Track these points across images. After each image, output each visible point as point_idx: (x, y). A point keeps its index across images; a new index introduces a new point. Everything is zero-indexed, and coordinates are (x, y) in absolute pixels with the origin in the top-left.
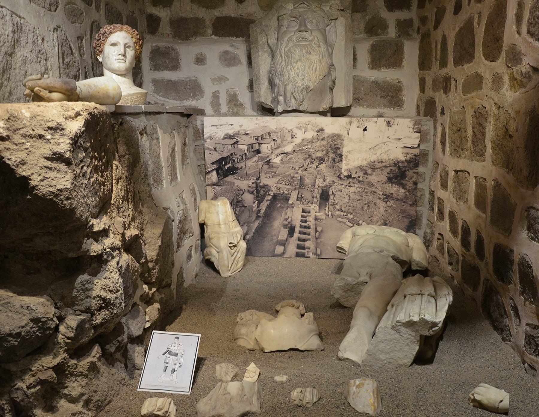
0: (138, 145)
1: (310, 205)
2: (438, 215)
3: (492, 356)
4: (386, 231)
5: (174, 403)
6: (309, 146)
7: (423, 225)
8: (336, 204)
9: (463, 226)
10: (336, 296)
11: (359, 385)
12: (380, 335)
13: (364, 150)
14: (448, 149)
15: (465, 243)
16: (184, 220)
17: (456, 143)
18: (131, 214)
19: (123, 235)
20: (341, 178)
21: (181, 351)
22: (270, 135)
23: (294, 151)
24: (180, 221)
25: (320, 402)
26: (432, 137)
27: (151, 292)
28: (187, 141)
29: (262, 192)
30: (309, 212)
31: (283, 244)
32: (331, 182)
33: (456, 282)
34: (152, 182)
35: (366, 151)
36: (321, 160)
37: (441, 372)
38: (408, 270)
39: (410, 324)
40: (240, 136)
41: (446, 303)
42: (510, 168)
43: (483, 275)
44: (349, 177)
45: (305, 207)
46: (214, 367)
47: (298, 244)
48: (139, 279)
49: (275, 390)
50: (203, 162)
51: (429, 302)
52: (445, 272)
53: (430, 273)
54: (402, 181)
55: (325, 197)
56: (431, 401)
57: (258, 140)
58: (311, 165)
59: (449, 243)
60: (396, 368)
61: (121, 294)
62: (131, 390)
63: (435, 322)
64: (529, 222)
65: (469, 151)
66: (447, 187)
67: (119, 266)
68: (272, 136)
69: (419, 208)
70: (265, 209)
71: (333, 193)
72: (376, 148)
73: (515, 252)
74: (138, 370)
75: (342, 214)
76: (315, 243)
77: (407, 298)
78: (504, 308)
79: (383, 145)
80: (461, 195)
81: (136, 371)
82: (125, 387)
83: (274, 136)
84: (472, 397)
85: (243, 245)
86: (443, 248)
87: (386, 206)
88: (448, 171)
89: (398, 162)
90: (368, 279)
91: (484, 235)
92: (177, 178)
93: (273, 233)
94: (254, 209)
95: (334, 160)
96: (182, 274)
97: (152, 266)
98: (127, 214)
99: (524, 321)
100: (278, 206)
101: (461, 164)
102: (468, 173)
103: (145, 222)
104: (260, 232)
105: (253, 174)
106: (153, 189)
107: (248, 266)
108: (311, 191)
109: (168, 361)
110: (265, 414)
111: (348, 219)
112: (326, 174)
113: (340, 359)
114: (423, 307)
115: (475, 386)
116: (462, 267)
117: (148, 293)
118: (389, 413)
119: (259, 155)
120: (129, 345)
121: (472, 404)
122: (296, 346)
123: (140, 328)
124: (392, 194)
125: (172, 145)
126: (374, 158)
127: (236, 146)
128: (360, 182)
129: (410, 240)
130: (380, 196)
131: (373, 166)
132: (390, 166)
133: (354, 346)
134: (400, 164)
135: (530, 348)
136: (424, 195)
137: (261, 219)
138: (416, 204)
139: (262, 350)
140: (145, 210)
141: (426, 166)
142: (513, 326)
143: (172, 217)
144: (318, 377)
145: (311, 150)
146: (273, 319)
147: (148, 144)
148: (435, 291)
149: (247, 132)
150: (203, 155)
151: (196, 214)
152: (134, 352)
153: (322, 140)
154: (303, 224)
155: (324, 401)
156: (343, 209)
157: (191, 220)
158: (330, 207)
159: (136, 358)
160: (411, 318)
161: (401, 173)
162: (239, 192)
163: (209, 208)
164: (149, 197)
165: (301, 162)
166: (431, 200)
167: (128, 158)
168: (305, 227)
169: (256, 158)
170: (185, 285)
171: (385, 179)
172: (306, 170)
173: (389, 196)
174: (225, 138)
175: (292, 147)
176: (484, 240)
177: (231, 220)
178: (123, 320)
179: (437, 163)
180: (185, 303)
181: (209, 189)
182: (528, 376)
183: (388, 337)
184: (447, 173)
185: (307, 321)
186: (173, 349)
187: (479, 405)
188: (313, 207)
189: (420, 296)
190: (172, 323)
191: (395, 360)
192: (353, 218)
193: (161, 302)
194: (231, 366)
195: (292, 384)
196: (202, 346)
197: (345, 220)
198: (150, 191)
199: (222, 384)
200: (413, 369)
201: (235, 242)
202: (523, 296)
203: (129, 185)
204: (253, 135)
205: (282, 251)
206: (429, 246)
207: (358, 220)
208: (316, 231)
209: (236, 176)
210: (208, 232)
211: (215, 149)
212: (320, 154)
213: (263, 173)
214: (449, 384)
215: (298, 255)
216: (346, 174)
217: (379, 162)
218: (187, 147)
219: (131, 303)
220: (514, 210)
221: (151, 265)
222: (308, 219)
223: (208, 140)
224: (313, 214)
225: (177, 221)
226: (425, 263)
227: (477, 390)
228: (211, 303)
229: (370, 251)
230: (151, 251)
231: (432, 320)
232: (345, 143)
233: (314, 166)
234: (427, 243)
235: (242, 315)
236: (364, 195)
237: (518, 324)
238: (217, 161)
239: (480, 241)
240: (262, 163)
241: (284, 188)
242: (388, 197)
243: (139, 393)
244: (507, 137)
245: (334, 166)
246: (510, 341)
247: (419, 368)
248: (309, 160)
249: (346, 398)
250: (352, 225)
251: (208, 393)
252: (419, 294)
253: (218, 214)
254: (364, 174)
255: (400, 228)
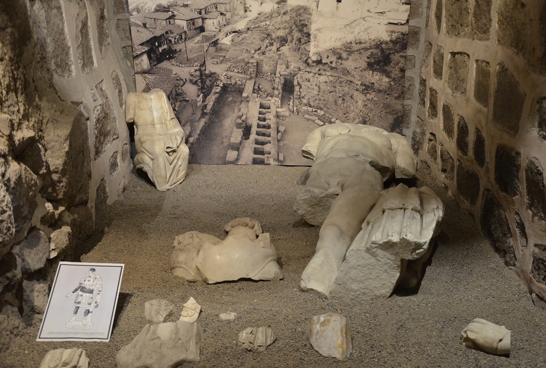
0: (25, 13)
1: (270, 98)
2: (430, 110)
3: (492, 284)
4: (364, 130)
5: (87, 354)
6: (268, 23)
7: (412, 123)
8: (303, 97)
9: (459, 123)
10: (300, 212)
11: (324, 322)
12: (352, 260)
13: (338, 27)
14: (444, 25)
15: (462, 145)
16: (104, 117)
17: (455, 17)
18: (22, 109)
19: (10, 137)
20: (308, 64)
21: (98, 286)
22: (216, 8)
23: (248, 29)
24: (98, 120)
25: (276, 345)
26: (425, 10)
27: (57, 212)
28: (106, 14)
29: (208, 83)
30: (269, 108)
31: (237, 148)
32: (296, 69)
33: (450, 193)
34: (53, 67)
35: (340, 28)
36: (283, 41)
37: (427, 304)
38: (390, 178)
39: (388, 246)
40: (177, 8)
41: (433, 220)
42: (520, 47)
43: (483, 183)
44: (319, 62)
45: (264, 102)
46: (142, 305)
47: (255, 148)
48: (39, 196)
49: (220, 330)
50: (129, 43)
51: (413, 218)
52: (437, 181)
53: (419, 183)
54: (386, 67)
55: (288, 88)
56: (413, 340)
57: (200, 13)
58: (270, 48)
59: (442, 145)
60: (372, 300)
61: (10, 216)
62: (28, 342)
63: (419, 243)
64: (541, 116)
65: (470, 27)
66: (441, 75)
67: (6, 178)
68: (219, 9)
69: (406, 102)
70: (212, 103)
71: (298, 83)
72: (353, 25)
73: (522, 155)
74: (38, 313)
75: (310, 109)
76: (276, 147)
77: (386, 213)
78: (508, 225)
79: (362, 21)
80: (458, 84)
81: (36, 315)
82: (18, 337)
83: (222, 8)
84: (465, 336)
85: (185, 150)
86: (436, 151)
87: (365, 99)
88: (443, 54)
89: (381, 43)
90: (339, 190)
91: (484, 134)
92: (92, 63)
93: (224, 135)
94: (199, 104)
95: (299, 40)
96: (105, 187)
97: (57, 179)
98: (16, 109)
99: (532, 241)
100: (230, 100)
101: (460, 44)
102: (468, 55)
103: (45, 121)
104: (207, 133)
105: (196, 59)
106: (56, 76)
107: (192, 177)
108: (271, 81)
109: (80, 300)
110: (206, 362)
111: (317, 116)
112: (289, 59)
113: (303, 291)
114: (405, 224)
115: (468, 322)
116: (458, 174)
117: (53, 213)
118: (361, 356)
119: (203, 34)
120: (25, 283)
121: (464, 344)
122: (248, 275)
123: (41, 259)
124: (373, 84)
125: (82, 17)
126: (350, 38)
127: (172, 21)
128: (332, 68)
129: (393, 141)
130: (358, 87)
131: (349, 49)
132: (371, 48)
133: (320, 274)
134: (383, 46)
135: (539, 274)
136: (414, 85)
137: (207, 117)
138: (403, 97)
139: (205, 281)
140: (44, 104)
141: (417, 48)
142: (518, 247)
143: (86, 115)
144: (275, 314)
145: (270, 28)
146: (219, 242)
147: (44, 15)
148: (422, 204)
149: (186, 3)
150: (128, 33)
151: (123, 111)
152: (32, 291)
153: (284, 14)
154: (262, 123)
155: (280, 344)
156: (312, 104)
157: (114, 118)
158: (296, 101)
159: (36, 298)
160: (390, 238)
161: (383, 57)
162: (179, 82)
163: (139, 103)
164: (50, 87)
165: (257, 43)
166: (422, 92)
167: (12, 32)
168: (264, 127)
169: (199, 38)
170: (109, 202)
171: (364, 65)
172: (264, 53)
173: (369, 87)
174: (157, 11)
175: (246, 23)
176: (484, 140)
177: (169, 118)
178: (16, 250)
179: (431, 44)
180: (108, 225)
181: (139, 77)
182: (536, 309)
183: (362, 262)
184: (442, 57)
185: (262, 244)
186: (88, 285)
187: (474, 345)
188: (273, 101)
189: (403, 210)
190: (89, 251)
191: (371, 290)
192: (324, 115)
193: (73, 225)
194: (164, 302)
195: (241, 323)
196: (126, 279)
197: (314, 118)
198: (51, 79)
199: (150, 327)
200: (393, 301)
201: (175, 146)
202: (531, 209)
203: (17, 69)
204: (194, 7)
205: (236, 157)
206: (418, 149)
207: (330, 117)
208: (278, 132)
209: (173, 61)
210: (139, 134)
211: (145, 25)
212: (281, 33)
213: (209, 58)
214: (437, 319)
215: (255, 162)
216: (314, 58)
217: (356, 44)
218: (106, 22)
219: (27, 227)
220: (523, 102)
221: (55, 177)
222: (267, 116)
223: (135, 13)
224: (273, 109)
225: (93, 120)
226: (411, 171)
227: (471, 326)
228: (142, 224)
229: (343, 155)
230: (55, 158)
231: (416, 240)
232: (314, 18)
233: (274, 48)
234: (416, 147)
235: (180, 238)
236: (337, 85)
237: (525, 244)
238: (147, 42)
239: (480, 142)
240: (208, 44)
241: (237, 77)
242: (367, 88)
243: (38, 344)
244: (519, 6)
245: (299, 48)
246: (514, 265)
247: (400, 300)
248: (267, 41)
249: (308, 339)
250: (322, 123)
251: (132, 339)
252: (401, 209)
253: (152, 111)
254: (338, 58)
255: (382, 127)
